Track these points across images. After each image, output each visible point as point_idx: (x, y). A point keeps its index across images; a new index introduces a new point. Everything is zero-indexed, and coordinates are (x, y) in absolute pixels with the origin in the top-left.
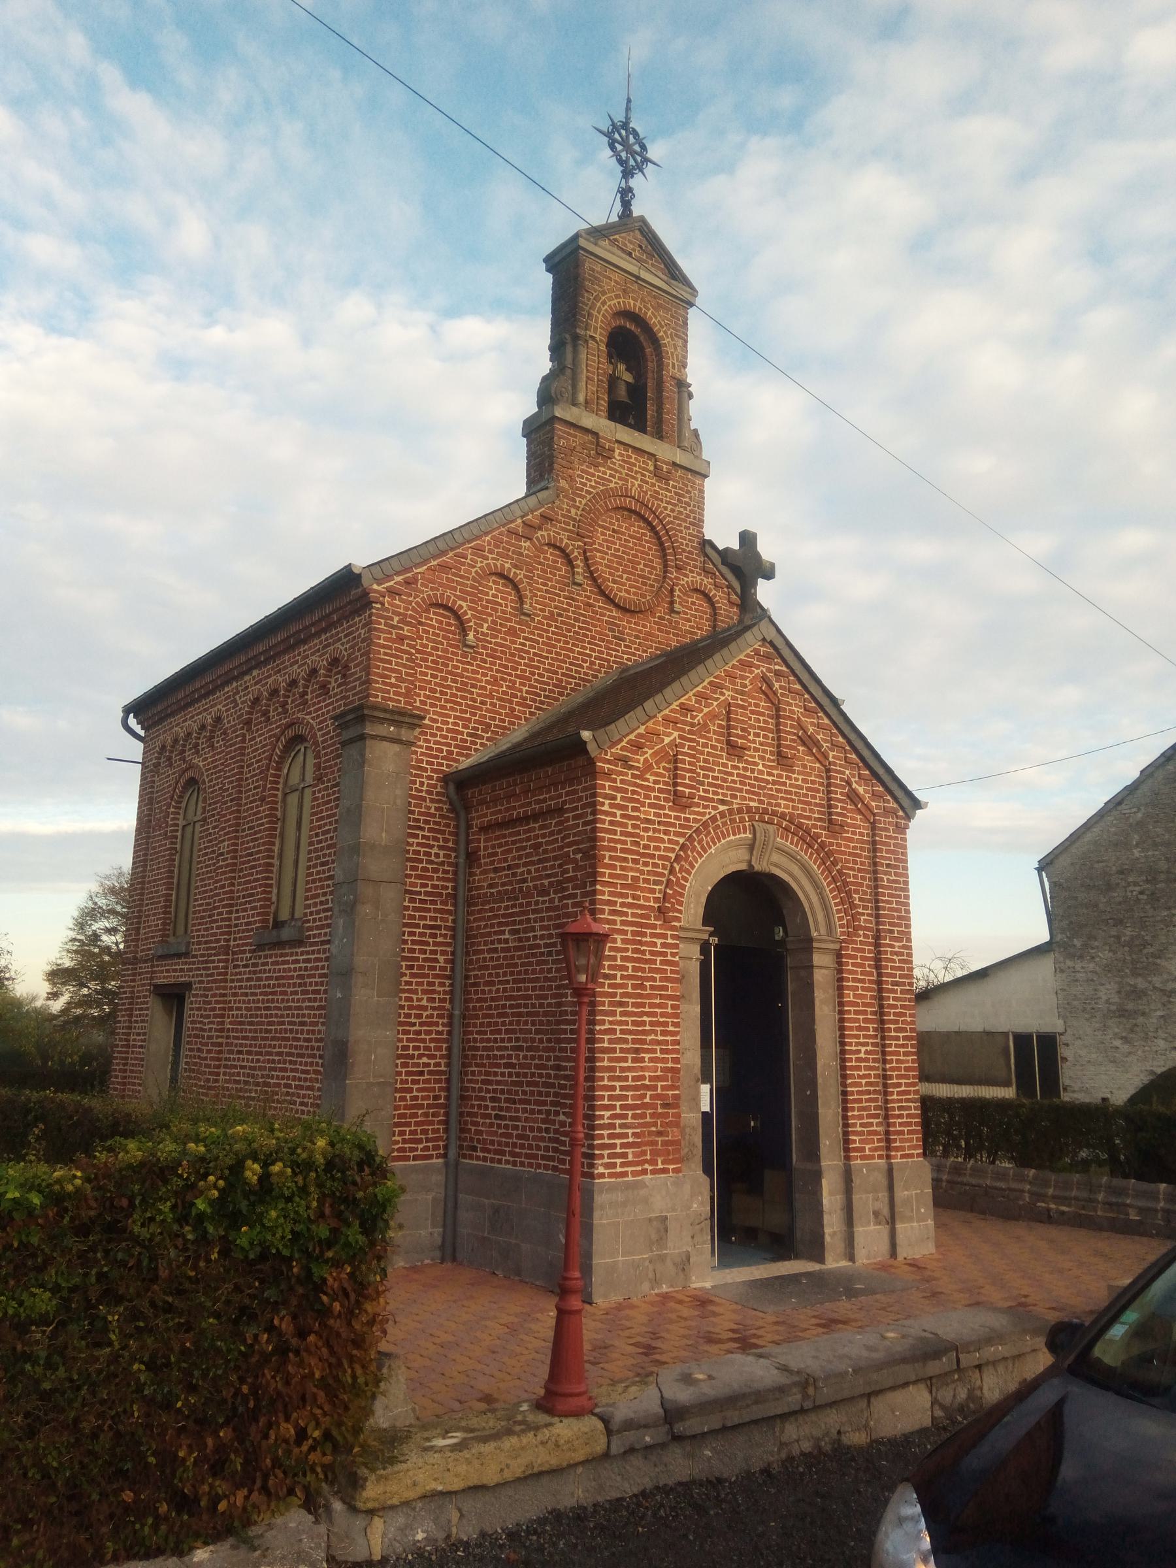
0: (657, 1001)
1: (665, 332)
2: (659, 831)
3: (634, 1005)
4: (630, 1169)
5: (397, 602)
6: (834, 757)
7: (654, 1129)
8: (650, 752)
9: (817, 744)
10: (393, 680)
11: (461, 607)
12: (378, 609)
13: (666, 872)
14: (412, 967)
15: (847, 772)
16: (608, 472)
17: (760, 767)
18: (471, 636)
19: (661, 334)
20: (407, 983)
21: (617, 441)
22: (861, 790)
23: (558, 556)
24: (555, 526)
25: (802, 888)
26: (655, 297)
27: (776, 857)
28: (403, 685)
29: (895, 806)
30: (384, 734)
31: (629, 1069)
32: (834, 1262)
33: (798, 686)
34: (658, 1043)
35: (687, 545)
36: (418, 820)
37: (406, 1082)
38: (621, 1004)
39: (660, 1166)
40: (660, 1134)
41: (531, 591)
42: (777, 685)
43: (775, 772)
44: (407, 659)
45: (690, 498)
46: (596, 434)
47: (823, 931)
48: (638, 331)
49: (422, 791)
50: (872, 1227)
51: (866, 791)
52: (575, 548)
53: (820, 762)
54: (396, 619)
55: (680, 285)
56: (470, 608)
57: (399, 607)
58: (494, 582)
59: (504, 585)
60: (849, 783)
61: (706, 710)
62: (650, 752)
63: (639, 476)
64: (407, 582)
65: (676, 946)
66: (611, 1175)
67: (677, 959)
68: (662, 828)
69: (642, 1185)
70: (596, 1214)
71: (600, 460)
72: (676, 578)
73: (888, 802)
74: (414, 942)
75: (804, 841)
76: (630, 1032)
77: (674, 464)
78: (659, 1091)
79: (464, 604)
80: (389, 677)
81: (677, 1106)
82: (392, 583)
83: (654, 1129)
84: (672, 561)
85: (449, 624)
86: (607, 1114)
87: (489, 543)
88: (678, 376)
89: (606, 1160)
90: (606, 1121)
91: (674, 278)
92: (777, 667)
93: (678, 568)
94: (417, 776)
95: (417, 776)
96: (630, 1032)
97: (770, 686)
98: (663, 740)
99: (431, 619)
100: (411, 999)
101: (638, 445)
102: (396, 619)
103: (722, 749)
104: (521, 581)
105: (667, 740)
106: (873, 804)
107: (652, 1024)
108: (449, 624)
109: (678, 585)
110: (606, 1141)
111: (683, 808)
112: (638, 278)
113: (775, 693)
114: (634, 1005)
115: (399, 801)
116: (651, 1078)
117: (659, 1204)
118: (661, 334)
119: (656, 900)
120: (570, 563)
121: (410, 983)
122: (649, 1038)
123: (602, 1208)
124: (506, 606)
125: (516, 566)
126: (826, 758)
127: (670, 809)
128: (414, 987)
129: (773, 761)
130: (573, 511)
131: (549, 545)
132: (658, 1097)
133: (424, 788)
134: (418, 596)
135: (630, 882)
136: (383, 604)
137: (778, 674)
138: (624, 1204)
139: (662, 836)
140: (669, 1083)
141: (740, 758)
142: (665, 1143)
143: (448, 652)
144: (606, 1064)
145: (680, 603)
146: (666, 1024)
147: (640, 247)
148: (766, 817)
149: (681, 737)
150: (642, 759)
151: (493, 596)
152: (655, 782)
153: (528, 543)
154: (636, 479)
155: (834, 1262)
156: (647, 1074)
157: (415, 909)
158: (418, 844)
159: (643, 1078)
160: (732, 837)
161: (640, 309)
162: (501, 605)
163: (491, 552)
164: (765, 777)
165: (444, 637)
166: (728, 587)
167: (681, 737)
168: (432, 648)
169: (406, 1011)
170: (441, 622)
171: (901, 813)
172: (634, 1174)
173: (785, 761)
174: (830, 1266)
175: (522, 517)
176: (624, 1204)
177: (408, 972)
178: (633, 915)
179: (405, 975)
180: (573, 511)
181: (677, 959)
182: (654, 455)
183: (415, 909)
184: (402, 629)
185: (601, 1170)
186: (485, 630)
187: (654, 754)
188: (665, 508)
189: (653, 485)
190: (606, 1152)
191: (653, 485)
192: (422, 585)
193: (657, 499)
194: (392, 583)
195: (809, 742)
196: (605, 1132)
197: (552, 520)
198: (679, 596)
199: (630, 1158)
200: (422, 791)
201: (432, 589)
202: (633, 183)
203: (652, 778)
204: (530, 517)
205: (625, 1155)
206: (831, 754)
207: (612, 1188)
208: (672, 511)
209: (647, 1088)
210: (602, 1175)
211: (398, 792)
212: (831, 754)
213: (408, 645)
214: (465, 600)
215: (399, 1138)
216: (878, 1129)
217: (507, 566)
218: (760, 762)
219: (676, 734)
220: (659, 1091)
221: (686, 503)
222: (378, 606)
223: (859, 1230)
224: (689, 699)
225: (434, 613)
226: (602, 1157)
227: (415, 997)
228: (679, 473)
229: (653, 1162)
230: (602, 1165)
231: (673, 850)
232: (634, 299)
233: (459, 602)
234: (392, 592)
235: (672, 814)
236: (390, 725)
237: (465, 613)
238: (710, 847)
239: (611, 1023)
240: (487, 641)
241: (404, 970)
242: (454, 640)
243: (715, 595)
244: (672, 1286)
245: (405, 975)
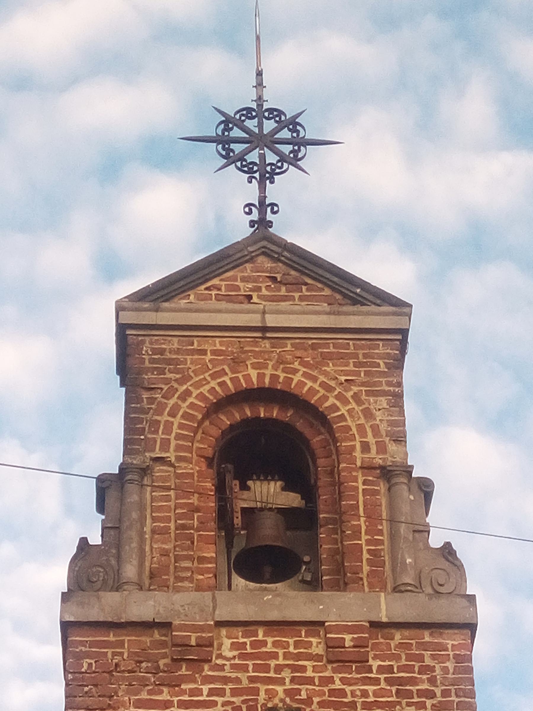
16: (205, 689)
21: (220, 624)
26: (314, 347)
63: (287, 674)
71: (184, 671)
77: (376, 625)
101: (274, 615)
112: (264, 329)
154: (281, 682)
182: (322, 624)
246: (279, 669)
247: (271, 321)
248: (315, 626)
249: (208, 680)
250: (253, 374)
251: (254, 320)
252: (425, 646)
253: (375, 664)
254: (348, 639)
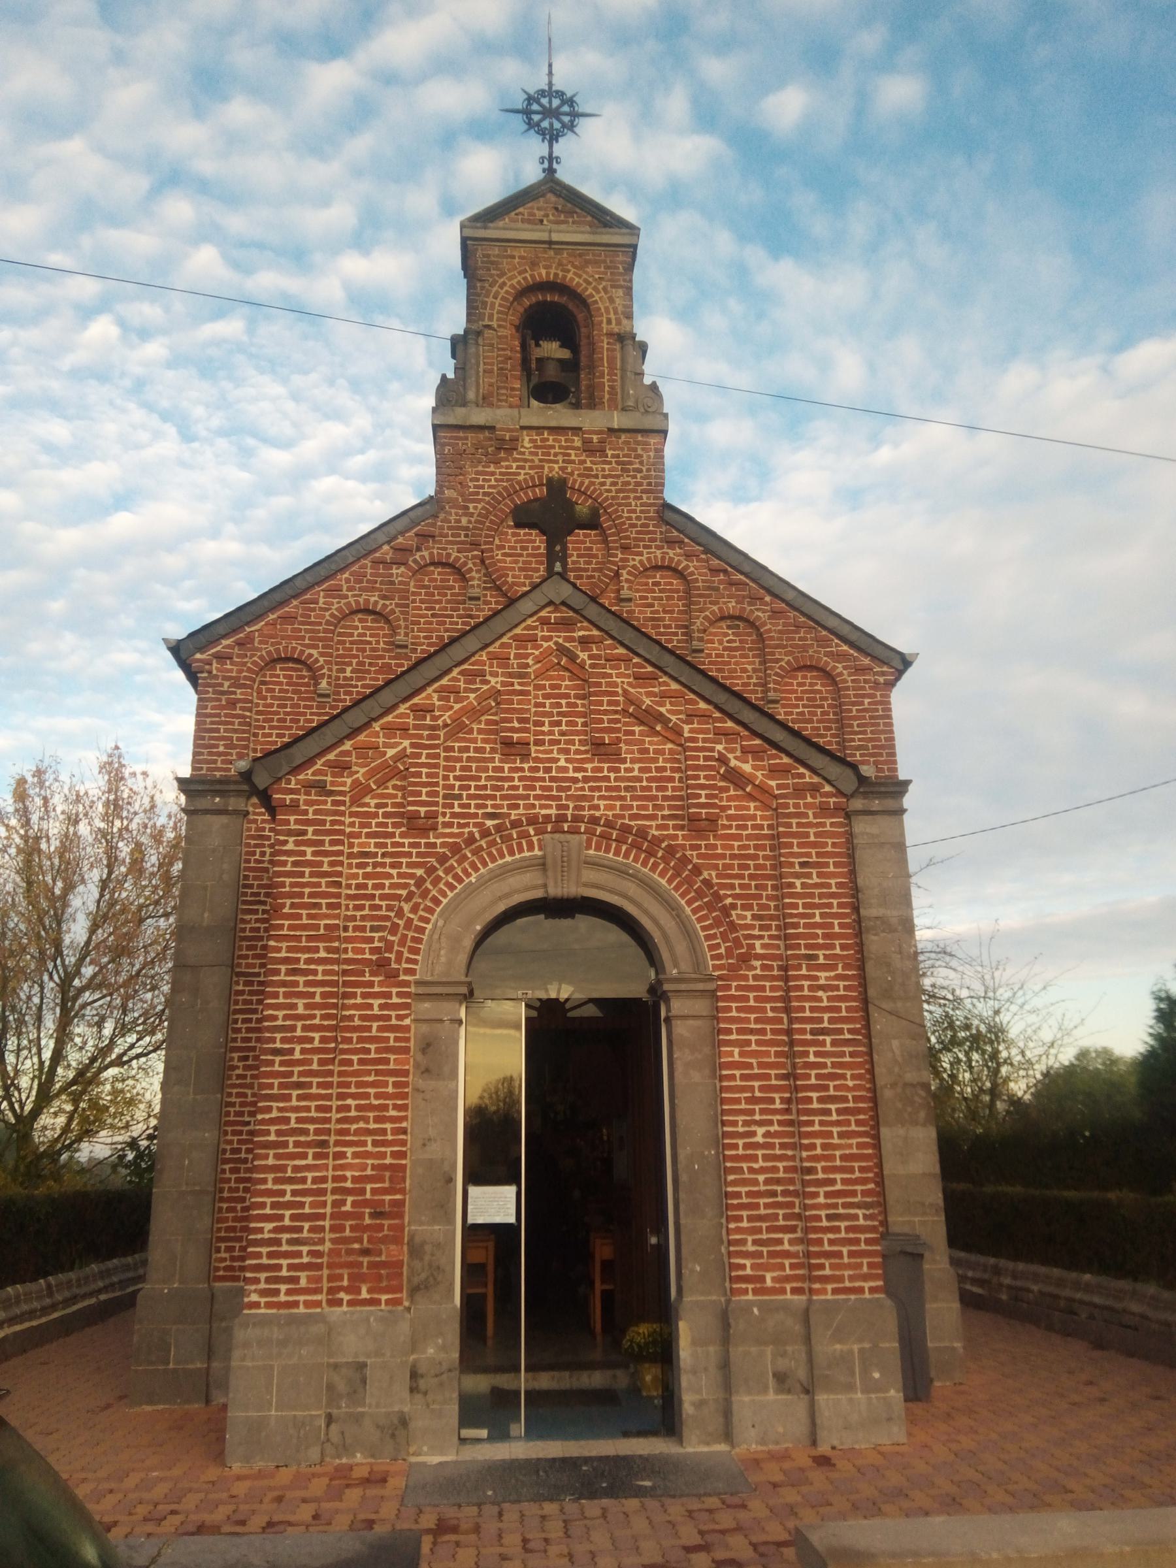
0: (371, 1079)
1: (595, 289)
2: (383, 865)
3: (319, 1085)
4: (302, 1298)
5: (229, 667)
6: (691, 731)
7: (356, 1246)
8: (363, 770)
9: (661, 718)
10: (221, 749)
11: (311, 655)
12: (204, 678)
13: (392, 914)
14: (246, 1058)
15: (719, 747)
16: (514, 465)
17: (562, 763)
18: (324, 684)
19: (590, 291)
20: (239, 1077)
21: (523, 428)
22: (747, 768)
23: (449, 574)
24: (440, 542)
25: (646, 912)
26: (580, 255)
27: (589, 875)
28: (234, 752)
29: (816, 779)
30: (209, 807)
31: (308, 1168)
32: (695, 1446)
33: (621, 651)
34: (369, 1132)
35: (638, 518)
36: (258, 894)
37: (237, 1190)
38: (299, 1085)
39: (364, 1295)
40: (365, 1252)
41: (406, 620)
42: (583, 656)
43: (589, 766)
44: (240, 724)
45: (641, 463)
46: (492, 428)
47: (686, 966)
48: (564, 300)
49: (263, 862)
50: (771, 1396)
51: (755, 767)
52: (468, 560)
53: (673, 742)
54: (227, 684)
55: (617, 230)
56: (322, 654)
57: (231, 671)
58: (361, 621)
59: (373, 621)
60: (723, 760)
61: (457, 706)
62: (363, 770)
63: (560, 458)
64: (240, 644)
65: (406, 1006)
66: (269, 1305)
67: (407, 1022)
68: (388, 860)
69: (321, 1318)
70: (237, 1354)
71: (502, 455)
72: (622, 560)
73: (802, 776)
74: (249, 1030)
75: (640, 849)
76: (312, 1120)
77: (611, 430)
78: (368, 1196)
79: (314, 652)
80: (217, 746)
81: (400, 1216)
82: (219, 648)
83: (356, 1246)
84: (615, 541)
85: (303, 677)
86: (269, 1226)
87: (348, 581)
88: (616, 330)
89: (262, 1286)
90: (266, 1236)
91: (606, 225)
92: (581, 633)
93: (625, 548)
94: (256, 846)
95: (256, 846)
96: (312, 1120)
97: (572, 658)
98: (385, 753)
99: (278, 676)
100: (245, 1095)
101: (553, 424)
102: (227, 684)
103: (493, 750)
104: (393, 612)
105: (391, 752)
106: (773, 783)
107: (359, 1108)
108: (303, 677)
109: (624, 568)
110: (265, 1261)
111: (424, 831)
112: (550, 243)
113: (582, 666)
114: (319, 1085)
115: (225, 877)
116: (355, 1179)
117: (351, 1346)
118: (590, 291)
119: (373, 951)
120: (460, 574)
121: (244, 1077)
122: (354, 1126)
123: (246, 1345)
124: (378, 642)
125: (384, 597)
126: (680, 733)
127: (402, 835)
128: (248, 1081)
129: (586, 752)
130: (464, 520)
131: (433, 564)
132: (366, 1203)
133: (267, 858)
134: (252, 656)
135: (322, 932)
136: (210, 672)
137: (585, 642)
138: (283, 1343)
139: (388, 870)
140: (387, 1185)
141: (525, 757)
142: (372, 1265)
143: (298, 706)
144: (271, 1161)
145: (630, 588)
146: (385, 1108)
147: (556, 209)
148: (566, 826)
149: (413, 745)
150: (349, 781)
151: (360, 635)
152: (378, 806)
153: (402, 569)
154: (557, 462)
155: (695, 1446)
156: (349, 1174)
157: (251, 993)
158: (257, 921)
159: (344, 1178)
160: (508, 859)
161: (556, 275)
162: (370, 643)
163: (350, 589)
164: (571, 774)
165: (294, 692)
166: (706, 551)
167: (413, 745)
168: (279, 706)
169: (237, 1109)
170: (291, 677)
171: (828, 788)
172: (307, 1304)
173: (602, 750)
174: (690, 1450)
175: (389, 542)
176: (283, 1343)
177: (241, 1064)
178: (325, 973)
179: (238, 1067)
180: (464, 520)
181: (407, 1022)
182: (580, 429)
183: (251, 993)
184: (235, 693)
185: (254, 1297)
186: (348, 674)
187: (370, 774)
188: (603, 484)
189: (583, 462)
190: (263, 1276)
191: (583, 462)
192: (260, 642)
193: (588, 476)
194: (219, 648)
195: (649, 719)
196: (264, 1250)
197: (433, 537)
198: (627, 581)
199: (303, 1283)
200: (263, 862)
201: (273, 644)
202: (558, 149)
203: (373, 802)
204: (400, 540)
205: (295, 1280)
206: (686, 728)
207: (264, 1321)
208: (614, 484)
209: (349, 1191)
210: (256, 1305)
211: (225, 866)
212: (686, 728)
213: (242, 709)
214: (315, 647)
215: (227, 1255)
216: (793, 1249)
217: (373, 599)
218: (564, 760)
219: (406, 743)
220: (368, 1196)
221: (635, 470)
222: (205, 675)
223: (743, 1401)
224: (429, 697)
225: (281, 669)
226: (256, 1281)
227: (249, 1092)
228: (623, 437)
229: (353, 1289)
230: (255, 1291)
231: (405, 886)
232: (546, 267)
233: (308, 651)
234: (220, 657)
235: (406, 841)
236: (214, 797)
237: (317, 661)
238: (468, 875)
239: (280, 1109)
240: (352, 686)
241: (235, 1063)
242: (306, 692)
243: (687, 567)
244: (373, 1456)
245: (238, 1067)
246: (556, 455)
247: (555, 237)
248: (576, 430)
249: (516, 460)
250: (544, 272)
251: (544, 236)
252: (638, 443)
253: (610, 453)
254: (595, 438)
